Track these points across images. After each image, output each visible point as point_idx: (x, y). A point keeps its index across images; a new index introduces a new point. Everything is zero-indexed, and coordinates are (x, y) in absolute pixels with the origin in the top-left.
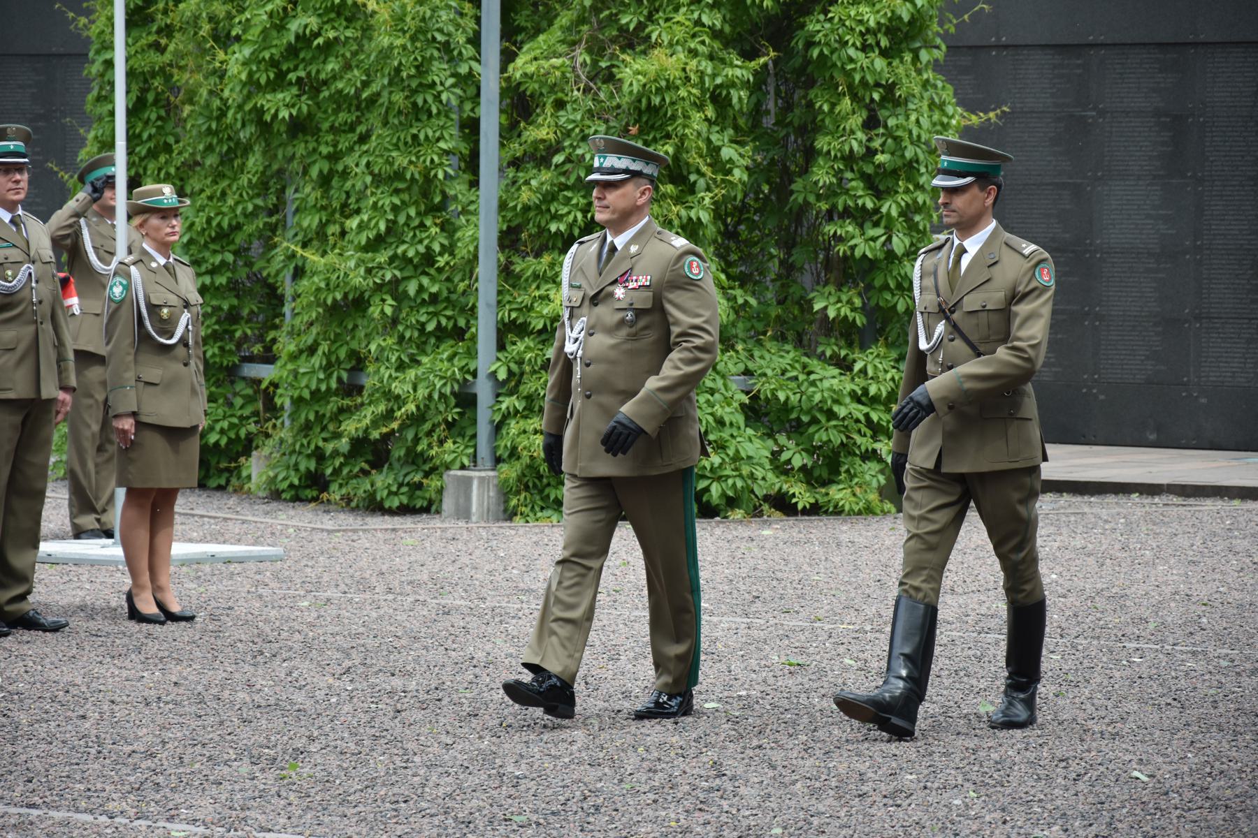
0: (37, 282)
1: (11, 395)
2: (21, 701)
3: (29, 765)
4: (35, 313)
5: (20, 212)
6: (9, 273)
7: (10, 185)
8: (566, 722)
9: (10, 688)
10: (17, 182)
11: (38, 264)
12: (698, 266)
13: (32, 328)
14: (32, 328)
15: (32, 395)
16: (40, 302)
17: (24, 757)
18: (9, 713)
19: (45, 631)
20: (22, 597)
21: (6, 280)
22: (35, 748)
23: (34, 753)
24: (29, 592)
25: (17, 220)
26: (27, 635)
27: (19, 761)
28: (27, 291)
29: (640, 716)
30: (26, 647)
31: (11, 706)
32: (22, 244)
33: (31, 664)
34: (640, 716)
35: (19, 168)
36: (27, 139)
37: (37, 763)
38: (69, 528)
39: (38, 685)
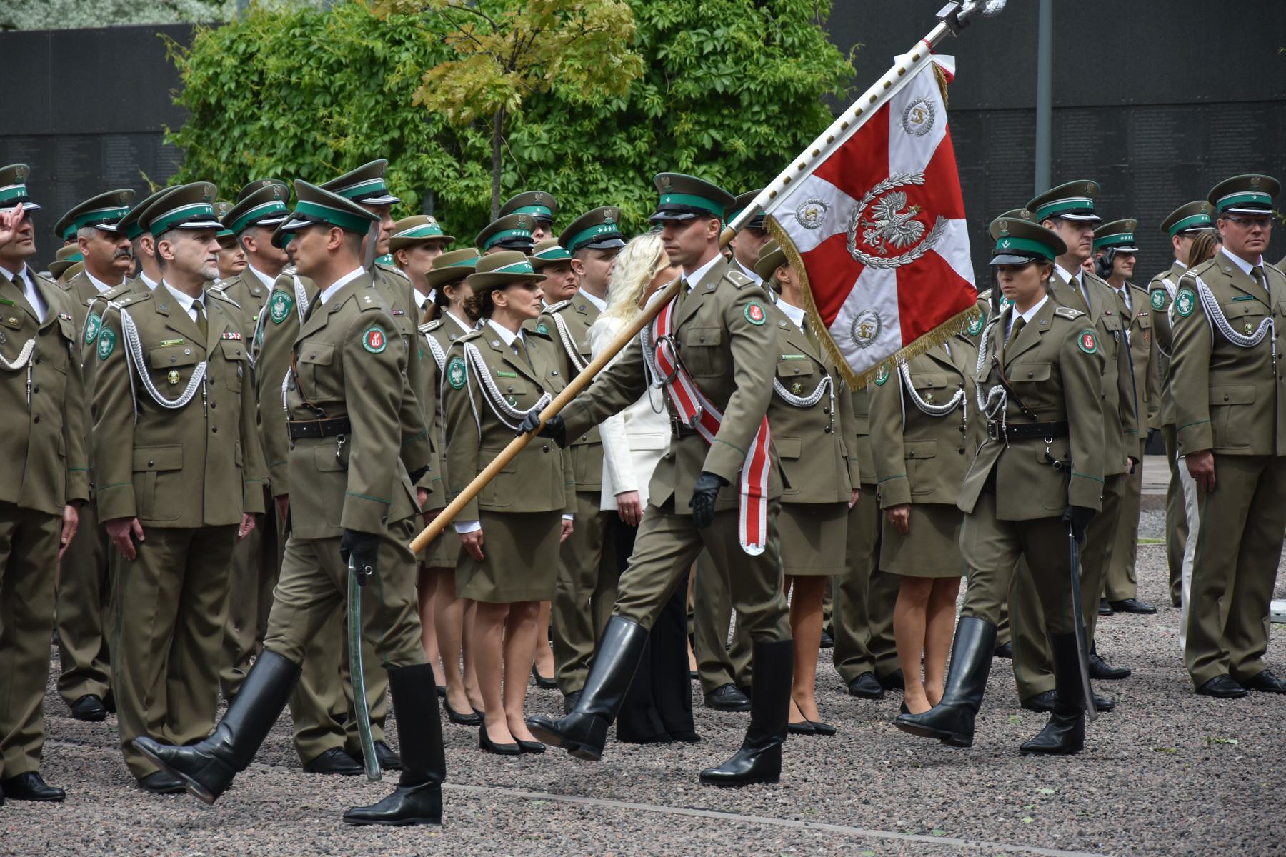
0: (1277, 336)
1: (1247, 451)
2: (1259, 764)
3: (1272, 830)
4: (1274, 367)
5: (1262, 264)
6: (1249, 326)
7: (1250, 237)
8: (960, 753)
9: (1248, 750)
10: (1257, 234)
11: (1279, 317)
12: (381, 337)
13: (1271, 383)
14: (1271, 383)
15: (1269, 452)
16: (1280, 356)
17: (1266, 822)
18: (1249, 777)
19: (1278, 693)
20: (1256, 656)
21: (1246, 334)
22: (1278, 813)
23: (1277, 818)
24: (1263, 652)
25: (1259, 271)
26: (1260, 697)
27: (1262, 826)
28: (1267, 344)
29: (1025, 751)
30: (1260, 709)
31: (1249, 769)
32: (1263, 297)
33: (1267, 726)
34: (1025, 751)
35: (1261, 220)
36: (1272, 189)
37: (1280, 828)
38: (433, 563)
39: (1276, 748)
